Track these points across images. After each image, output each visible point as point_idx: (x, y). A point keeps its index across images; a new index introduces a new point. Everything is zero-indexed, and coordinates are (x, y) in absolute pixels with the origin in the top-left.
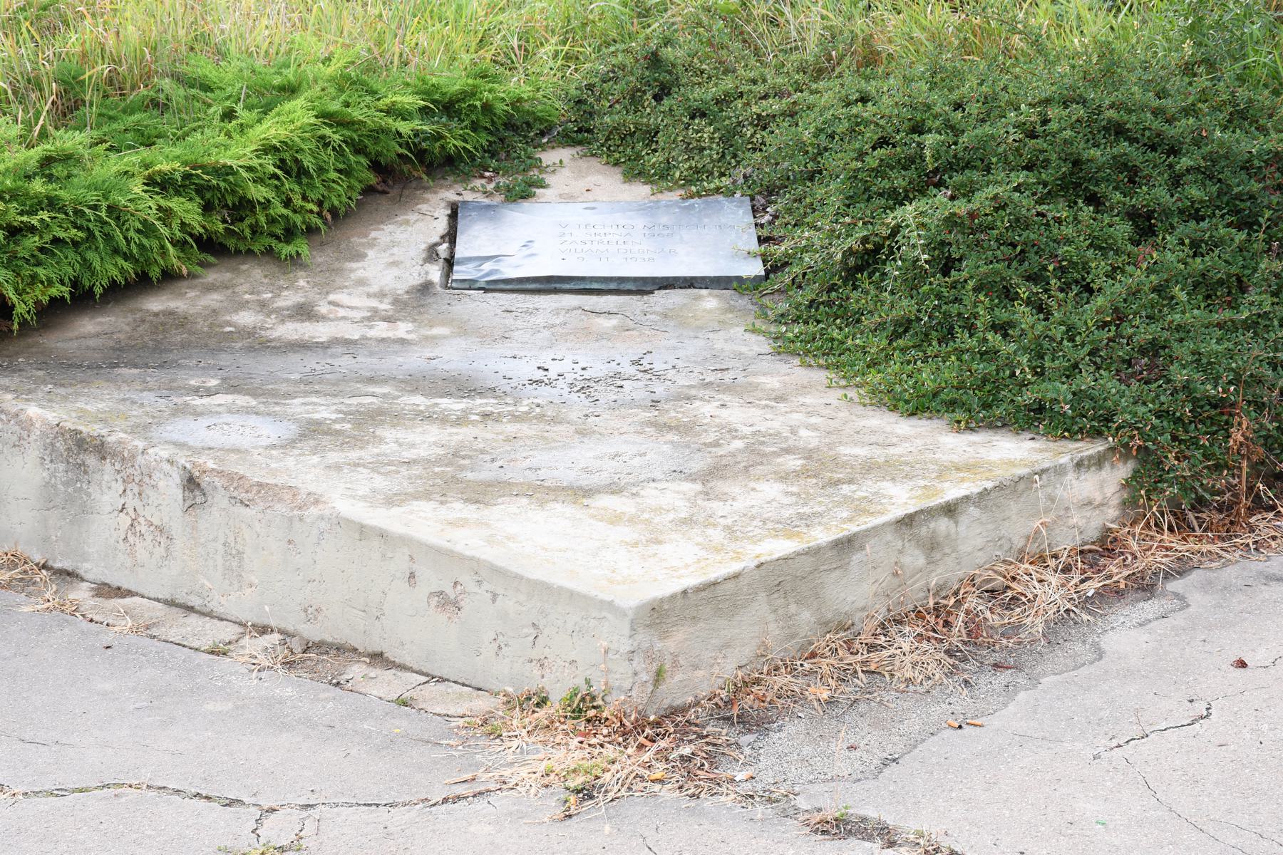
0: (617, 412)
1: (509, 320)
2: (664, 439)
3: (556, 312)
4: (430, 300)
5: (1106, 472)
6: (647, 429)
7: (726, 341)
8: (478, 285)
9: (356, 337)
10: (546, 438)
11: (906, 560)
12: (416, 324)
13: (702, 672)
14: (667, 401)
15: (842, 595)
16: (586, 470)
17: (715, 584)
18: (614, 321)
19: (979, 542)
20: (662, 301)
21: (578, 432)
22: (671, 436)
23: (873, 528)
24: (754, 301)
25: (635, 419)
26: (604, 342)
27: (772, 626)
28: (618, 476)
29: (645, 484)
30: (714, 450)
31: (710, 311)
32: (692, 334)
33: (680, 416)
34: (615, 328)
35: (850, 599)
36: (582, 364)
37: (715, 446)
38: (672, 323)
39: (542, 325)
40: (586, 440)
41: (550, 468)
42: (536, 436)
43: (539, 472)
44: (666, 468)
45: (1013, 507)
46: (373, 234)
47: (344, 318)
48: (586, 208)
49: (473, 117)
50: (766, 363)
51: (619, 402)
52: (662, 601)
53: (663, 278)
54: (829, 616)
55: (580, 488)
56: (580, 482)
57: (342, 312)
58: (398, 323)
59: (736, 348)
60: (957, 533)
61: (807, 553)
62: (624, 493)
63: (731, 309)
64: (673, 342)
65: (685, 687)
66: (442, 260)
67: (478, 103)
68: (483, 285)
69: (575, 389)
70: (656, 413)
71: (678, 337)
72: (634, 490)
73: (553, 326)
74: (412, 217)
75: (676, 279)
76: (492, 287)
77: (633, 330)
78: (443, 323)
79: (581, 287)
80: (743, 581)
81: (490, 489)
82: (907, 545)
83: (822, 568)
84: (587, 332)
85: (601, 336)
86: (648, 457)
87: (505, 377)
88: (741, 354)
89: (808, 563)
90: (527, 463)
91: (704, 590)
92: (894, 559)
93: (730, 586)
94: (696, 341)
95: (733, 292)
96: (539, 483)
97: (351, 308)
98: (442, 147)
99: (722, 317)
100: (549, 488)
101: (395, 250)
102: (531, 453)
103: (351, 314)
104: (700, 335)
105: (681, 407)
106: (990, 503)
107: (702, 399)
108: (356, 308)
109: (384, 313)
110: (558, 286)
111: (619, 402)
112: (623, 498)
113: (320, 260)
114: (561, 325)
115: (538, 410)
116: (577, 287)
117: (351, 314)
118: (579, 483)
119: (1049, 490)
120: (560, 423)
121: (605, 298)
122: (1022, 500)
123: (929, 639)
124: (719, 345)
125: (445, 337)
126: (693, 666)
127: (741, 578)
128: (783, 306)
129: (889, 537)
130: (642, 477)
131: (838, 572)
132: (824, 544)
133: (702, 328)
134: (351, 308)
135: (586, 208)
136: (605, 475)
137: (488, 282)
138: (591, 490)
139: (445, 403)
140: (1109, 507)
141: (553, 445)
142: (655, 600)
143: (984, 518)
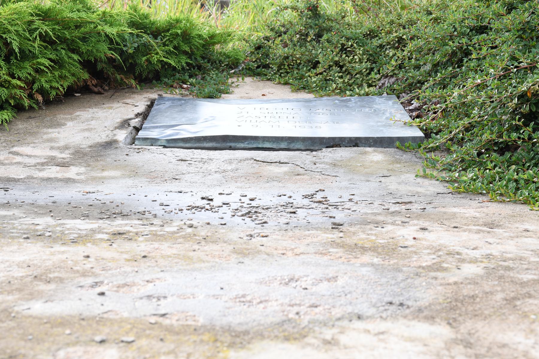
0: (290, 233)
1: (183, 167)
2: (358, 262)
3: (230, 162)
4: (112, 152)
6: (331, 250)
7: (399, 183)
8: (159, 143)
9: (22, 177)
10: (190, 258)
12: (89, 168)
14: (351, 225)
16: (242, 299)
18: (285, 168)
20: (330, 155)
21: (235, 251)
22: (366, 258)
24: (418, 155)
25: (315, 240)
26: (275, 183)
28: (296, 309)
29: (345, 323)
30: (439, 274)
31: (377, 162)
32: (363, 178)
33: (373, 238)
34: (285, 173)
36: (250, 196)
37: (438, 270)
38: (342, 171)
39: (213, 170)
40: (246, 260)
41: (183, 297)
42: (177, 256)
43: (163, 302)
44: (374, 298)
46: (78, 113)
47: (19, 163)
49: (175, 42)
50: (449, 199)
51: (292, 225)
53: (329, 138)
55: (228, 330)
56: (230, 319)
57: (18, 159)
58: (72, 167)
59: (410, 188)
62: (310, 340)
63: (398, 162)
64: (345, 184)
66: (131, 128)
67: (179, 32)
69: (240, 214)
70: (341, 235)
71: (350, 180)
72: (328, 334)
73: (225, 171)
74: (115, 105)
75: (342, 139)
77: (304, 175)
78: (116, 168)
81: (56, 330)
84: (258, 176)
85: (271, 179)
86: (340, 282)
87: (162, 205)
88: (418, 193)
90: (150, 289)
94: (368, 183)
95: (396, 149)
96: (153, 320)
97: (30, 156)
98: (148, 60)
99: (391, 167)
100: (170, 330)
101: (93, 122)
102: (161, 275)
103: (27, 160)
104: (371, 179)
105: (371, 229)
107: (393, 224)
108: (35, 156)
109: (59, 160)
111: (292, 225)
112: (308, 350)
113: (20, 126)
114: (232, 170)
115: (190, 230)
117: (27, 160)
118: (225, 321)
120: (215, 242)
124: (393, 187)
125: (113, 178)
128: (448, 159)
130: (337, 312)
133: (372, 174)
134: (30, 156)
136: (273, 306)
138: (246, 333)
139: (71, 223)
141: (197, 265)
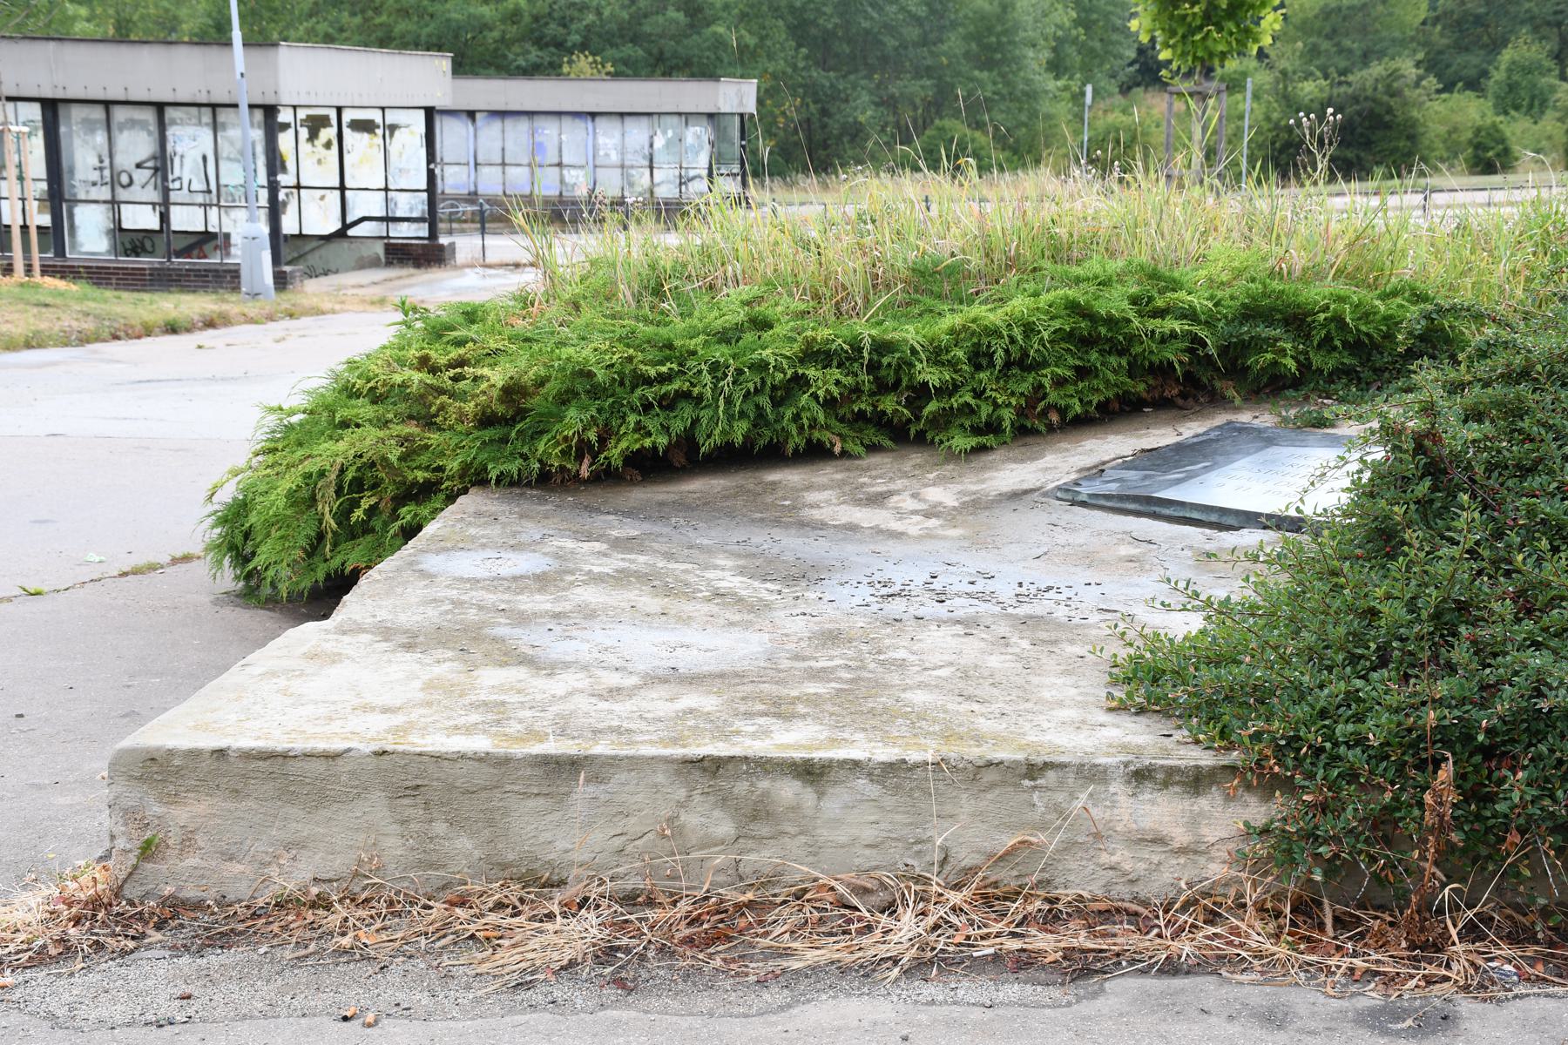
5: (1208, 803)
11: (690, 819)
13: (241, 867)
15: (547, 836)
17: (285, 756)
19: (869, 834)
23: (627, 757)
27: (391, 842)
35: (561, 845)
45: (966, 804)
48: (205, 158)
52: (171, 753)
54: (511, 857)
60: (817, 808)
61: (480, 760)
65: (203, 877)
68: (1085, 498)
76: (1093, 502)
79: (1181, 514)
80: (342, 766)
82: (697, 798)
83: (508, 788)
89: (484, 774)
91: (265, 759)
92: (665, 812)
93: (319, 767)
106: (908, 785)
110: (1157, 509)
116: (1176, 514)
119: (1060, 797)
121: (1157, 523)
122: (989, 796)
123: (874, 970)
126: (222, 854)
127: (340, 762)
129: (660, 778)
131: (541, 801)
132: (520, 756)
135: (205, 158)
137: (1091, 496)
140: (1212, 859)
142: (158, 749)
143: (889, 801)
